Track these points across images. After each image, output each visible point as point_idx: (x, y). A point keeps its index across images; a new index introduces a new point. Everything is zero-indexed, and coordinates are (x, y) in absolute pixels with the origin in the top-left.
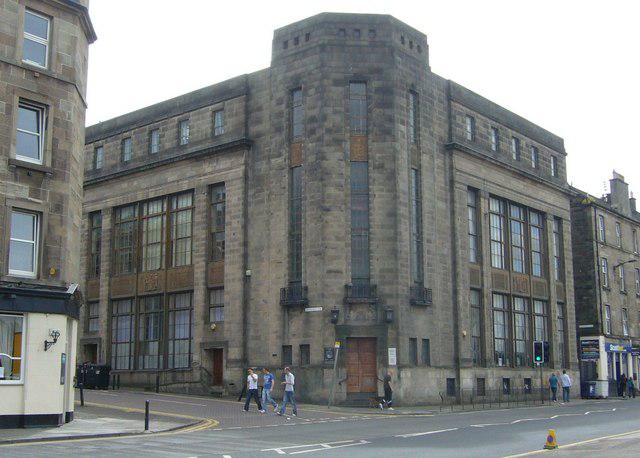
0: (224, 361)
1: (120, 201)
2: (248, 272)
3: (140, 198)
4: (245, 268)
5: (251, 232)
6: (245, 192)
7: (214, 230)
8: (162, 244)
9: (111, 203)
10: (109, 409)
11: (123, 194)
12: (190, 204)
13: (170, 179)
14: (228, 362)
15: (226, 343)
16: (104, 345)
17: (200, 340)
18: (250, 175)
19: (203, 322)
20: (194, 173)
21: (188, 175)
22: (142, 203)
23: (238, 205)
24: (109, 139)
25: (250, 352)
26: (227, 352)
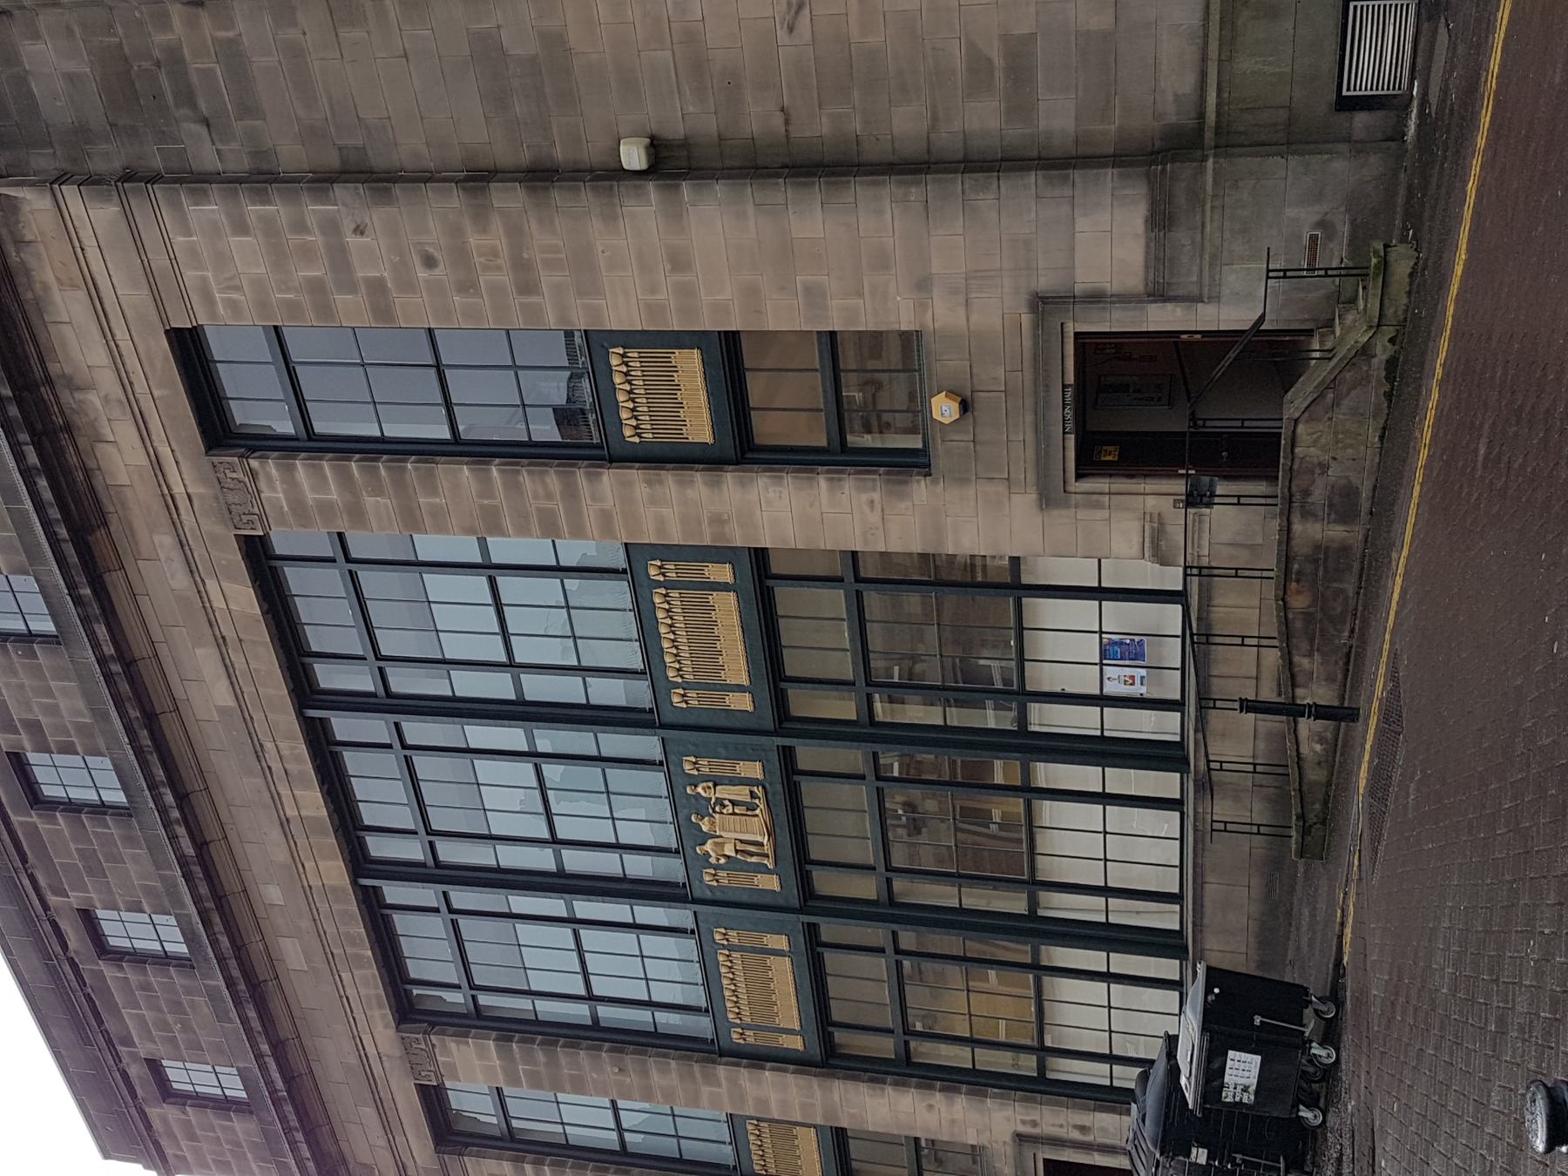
0: (1162, 318)
1: (366, 982)
2: (633, 156)
3: (334, 871)
4: (611, 174)
5: (410, 148)
6: (196, 180)
7: (1223, 57)
8: (1040, 969)
9: (381, 1031)
10: (961, 922)
11: (330, 957)
12: (835, 601)
13: (223, 695)
14: (1158, 293)
15: (1043, 305)
16: (1056, 1120)
17: (1024, 502)
18: (109, 157)
19: (920, 489)
20: (165, 541)
21: (180, 580)
22: (360, 863)
23: (270, 228)
24: (110, 1025)
25: (1108, 130)
26: (1096, 298)
